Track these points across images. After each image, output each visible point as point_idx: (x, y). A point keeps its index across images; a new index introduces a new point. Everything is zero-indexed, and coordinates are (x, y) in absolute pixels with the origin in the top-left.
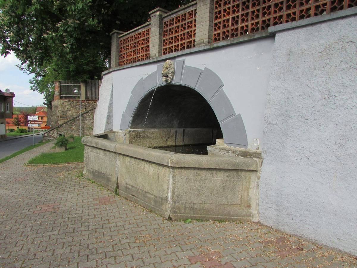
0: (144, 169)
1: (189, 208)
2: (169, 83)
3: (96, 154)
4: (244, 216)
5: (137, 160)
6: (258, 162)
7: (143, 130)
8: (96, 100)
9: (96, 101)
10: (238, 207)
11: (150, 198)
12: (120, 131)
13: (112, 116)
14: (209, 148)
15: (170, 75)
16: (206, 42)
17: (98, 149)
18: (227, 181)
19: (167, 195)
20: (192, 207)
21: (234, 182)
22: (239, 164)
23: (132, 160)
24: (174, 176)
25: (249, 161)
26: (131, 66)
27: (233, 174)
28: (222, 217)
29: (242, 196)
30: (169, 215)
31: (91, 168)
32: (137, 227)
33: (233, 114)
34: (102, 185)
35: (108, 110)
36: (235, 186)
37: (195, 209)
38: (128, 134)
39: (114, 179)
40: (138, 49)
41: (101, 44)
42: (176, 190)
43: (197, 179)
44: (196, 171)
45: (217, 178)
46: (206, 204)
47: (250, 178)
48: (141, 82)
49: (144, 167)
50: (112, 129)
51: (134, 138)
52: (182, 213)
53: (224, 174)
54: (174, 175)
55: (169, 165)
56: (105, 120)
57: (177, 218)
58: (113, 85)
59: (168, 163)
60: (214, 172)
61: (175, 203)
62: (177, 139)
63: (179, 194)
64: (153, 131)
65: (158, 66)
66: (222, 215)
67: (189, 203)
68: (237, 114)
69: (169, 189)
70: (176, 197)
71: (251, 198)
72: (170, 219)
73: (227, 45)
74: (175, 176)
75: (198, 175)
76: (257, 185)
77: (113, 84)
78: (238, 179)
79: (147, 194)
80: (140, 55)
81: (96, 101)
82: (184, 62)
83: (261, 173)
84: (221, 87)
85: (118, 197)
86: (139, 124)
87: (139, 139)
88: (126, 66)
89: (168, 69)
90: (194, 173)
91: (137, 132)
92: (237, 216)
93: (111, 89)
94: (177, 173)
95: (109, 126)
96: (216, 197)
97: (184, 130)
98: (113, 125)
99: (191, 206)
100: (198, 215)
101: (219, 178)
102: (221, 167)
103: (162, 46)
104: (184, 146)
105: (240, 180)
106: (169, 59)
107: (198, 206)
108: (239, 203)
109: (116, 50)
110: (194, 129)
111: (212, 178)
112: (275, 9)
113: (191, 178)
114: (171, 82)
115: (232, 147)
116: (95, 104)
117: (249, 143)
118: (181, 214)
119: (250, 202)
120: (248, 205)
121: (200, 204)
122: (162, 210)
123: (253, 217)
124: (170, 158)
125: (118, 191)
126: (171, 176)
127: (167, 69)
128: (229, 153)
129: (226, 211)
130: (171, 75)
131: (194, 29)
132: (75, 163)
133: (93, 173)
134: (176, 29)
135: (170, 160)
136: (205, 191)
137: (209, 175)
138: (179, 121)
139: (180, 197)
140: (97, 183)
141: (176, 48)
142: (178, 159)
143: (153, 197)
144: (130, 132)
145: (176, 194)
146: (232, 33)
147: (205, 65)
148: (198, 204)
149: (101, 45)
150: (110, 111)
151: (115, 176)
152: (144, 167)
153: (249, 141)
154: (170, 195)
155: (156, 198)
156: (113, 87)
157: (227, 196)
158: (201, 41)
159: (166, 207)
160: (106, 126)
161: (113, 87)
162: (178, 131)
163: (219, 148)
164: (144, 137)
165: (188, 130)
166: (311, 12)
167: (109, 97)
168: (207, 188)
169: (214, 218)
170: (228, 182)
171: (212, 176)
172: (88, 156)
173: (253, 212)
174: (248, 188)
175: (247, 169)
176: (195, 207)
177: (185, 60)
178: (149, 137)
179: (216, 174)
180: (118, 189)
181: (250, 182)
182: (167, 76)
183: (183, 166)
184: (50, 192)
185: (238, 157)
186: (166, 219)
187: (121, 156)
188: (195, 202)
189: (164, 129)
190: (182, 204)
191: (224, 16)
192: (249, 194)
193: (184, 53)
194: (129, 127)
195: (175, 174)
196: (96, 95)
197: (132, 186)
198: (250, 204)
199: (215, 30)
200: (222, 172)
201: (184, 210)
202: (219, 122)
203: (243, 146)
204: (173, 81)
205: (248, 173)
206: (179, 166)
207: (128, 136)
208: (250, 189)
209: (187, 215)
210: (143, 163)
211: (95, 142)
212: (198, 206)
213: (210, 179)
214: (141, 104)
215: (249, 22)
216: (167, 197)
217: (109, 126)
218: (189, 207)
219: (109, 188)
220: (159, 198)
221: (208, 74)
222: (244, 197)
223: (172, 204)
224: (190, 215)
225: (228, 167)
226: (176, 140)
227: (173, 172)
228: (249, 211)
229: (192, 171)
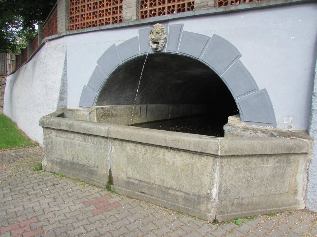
0: (164, 159)
1: (237, 204)
2: (160, 51)
3: (66, 140)
4: (290, 205)
5: (151, 147)
6: (309, 144)
7: (110, 107)
8: (4, 74)
9: (4, 77)
10: (286, 195)
11: (176, 197)
12: (80, 109)
13: (66, 91)
14: (228, 128)
15: (162, 42)
16: (211, 5)
17: (70, 133)
18: (277, 167)
19: (209, 192)
20: (240, 203)
21: (284, 168)
22: (292, 148)
23: (139, 147)
24: (221, 168)
25: (301, 143)
26: (96, 30)
27: (283, 158)
28: (271, 209)
29: (289, 183)
30: (214, 217)
31: (58, 158)
32: (113, 222)
33: (256, 89)
34: (79, 180)
35: (61, 83)
36: (284, 172)
37: (244, 204)
38: (95, 112)
39: (103, 172)
40: (76, 16)
41: (20, 9)
42: (224, 184)
43: (247, 168)
44: (247, 158)
45: (267, 165)
46: (254, 197)
47: (298, 162)
48: (112, 50)
49: (164, 155)
50: (67, 107)
51: (104, 117)
52: (229, 212)
53: (274, 159)
54: (221, 166)
55: (219, 154)
56: (57, 95)
57: (223, 219)
58: (66, 53)
59: (217, 151)
60: (265, 158)
61: (222, 201)
62: (141, 116)
63: (227, 190)
64: (120, 108)
65: (139, 30)
66: (269, 208)
67: (237, 199)
68: (260, 90)
69: (213, 184)
70: (223, 192)
71: (298, 184)
72: (215, 221)
73: (251, 8)
74: (223, 167)
75: (249, 163)
76: (305, 168)
77: (66, 51)
78: (288, 164)
79: (170, 191)
80: (104, 18)
81: (4, 77)
82: (182, 27)
83: (312, 155)
84: (238, 57)
85: (116, 196)
86: (105, 100)
87: (107, 118)
88: (89, 30)
89: (160, 34)
90: (244, 162)
91: (104, 110)
92: (284, 206)
93: (64, 58)
94: (225, 164)
95: (62, 103)
96: (265, 187)
97: (147, 106)
98: (67, 101)
99: (238, 202)
100: (247, 212)
101: (270, 165)
102: (275, 151)
103: (139, 8)
104: (147, 123)
105: (289, 164)
106: (160, 22)
107: (247, 201)
108: (287, 191)
109: (65, 10)
110: (154, 106)
111: (263, 166)
112: (93, 16)
113: (241, 167)
114: (162, 50)
115: (253, 126)
116: (3, 79)
117: (277, 121)
118: (228, 213)
119: (297, 188)
120: (295, 191)
121: (248, 197)
122: (201, 210)
123: (299, 205)
124: (219, 144)
125: (113, 187)
126: (218, 168)
127: (159, 34)
128: (257, 134)
129: (274, 202)
130: (163, 41)
131: (121, 5)
132: (12, 150)
133: (63, 164)
134: (82, 8)
135: (221, 148)
136: (255, 182)
137: (260, 163)
138: (141, 97)
139: (227, 193)
140: (70, 176)
141: (107, 21)
142: (230, 146)
143: (183, 194)
144: (97, 109)
145: (223, 189)
146: (106, 21)
147: (213, 32)
148: (246, 198)
149: (21, 10)
150: (63, 84)
151: (106, 167)
152: (164, 155)
153: (278, 119)
154: (215, 192)
155: (187, 196)
156: (66, 54)
157: (276, 184)
158: (203, 3)
159: (207, 206)
160: (59, 103)
161: (66, 54)
162: (142, 108)
163: (242, 128)
164: (112, 115)
165: (151, 106)
166: (166, 11)
167: (62, 66)
168: (257, 178)
169: (263, 212)
170: (278, 169)
171: (263, 163)
172: (51, 142)
173: (299, 199)
174: (296, 173)
175: (299, 152)
176: (244, 202)
177: (183, 24)
178: (116, 116)
179: (267, 160)
180: (113, 184)
181: (298, 166)
182: (158, 43)
183: (235, 154)
184: (6, 199)
185: (280, 138)
186: (210, 223)
187: (117, 142)
188: (244, 196)
189: (130, 105)
190: (230, 200)
191: (100, 7)
192: (297, 180)
193: (184, 16)
194: (94, 103)
195: (223, 165)
196: (4, 70)
197: (140, 181)
198: (296, 190)
199: (142, 7)
200: (273, 157)
201: (232, 208)
202: (235, 98)
203: (270, 125)
204: (164, 50)
205: (297, 156)
206: (231, 155)
207: (95, 114)
208: (298, 173)
209: (235, 214)
210: (162, 150)
211: (67, 124)
212: (247, 201)
213: (261, 167)
214: (111, 76)
215: (165, 5)
216: (208, 194)
217: (62, 103)
218: (236, 203)
219: (95, 183)
220: (194, 195)
221: (219, 42)
222: (291, 183)
223: (218, 203)
224: (238, 213)
225: (282, 152)
226: (140, 117)
227: (221, 162)
228: (296, 198)
229: (243, 159)
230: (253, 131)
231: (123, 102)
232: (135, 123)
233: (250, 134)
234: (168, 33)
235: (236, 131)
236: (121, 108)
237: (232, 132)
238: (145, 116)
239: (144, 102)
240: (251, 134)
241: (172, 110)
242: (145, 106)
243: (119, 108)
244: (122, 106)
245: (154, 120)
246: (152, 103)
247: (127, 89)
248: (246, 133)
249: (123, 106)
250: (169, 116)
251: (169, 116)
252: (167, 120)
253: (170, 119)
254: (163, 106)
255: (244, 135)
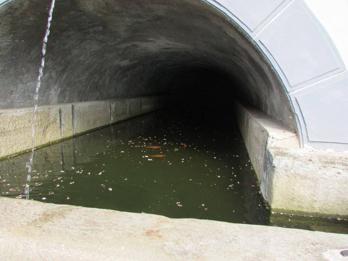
62: (63, 126)
64: (13, 116)
97: (73, 107)
115: (329, 150)
162: (63, 110)
226: (61, 127)
230: (344, 167)
231: (21, 102)
232: (51, 141)
233: (337, 175)
234: (32, 195)
235: (304, 169)
236: (15, 114)
237: (292, 171)
238: (71, 124)
239: (67, 98)
240: (338, 173)
241: (116, 108)
242: (69, 106)
243: (10, 115)
244: (16, 111)
245: (88, 129)
246: (81, 101)
247: (26, 75)
248: (327, 173)
249: (19, 110)
250: (112, 119)
251: (112, 119)
252: (108, 126)
253: (113, 124)
254: (101, 104)
255: (323, 176)
